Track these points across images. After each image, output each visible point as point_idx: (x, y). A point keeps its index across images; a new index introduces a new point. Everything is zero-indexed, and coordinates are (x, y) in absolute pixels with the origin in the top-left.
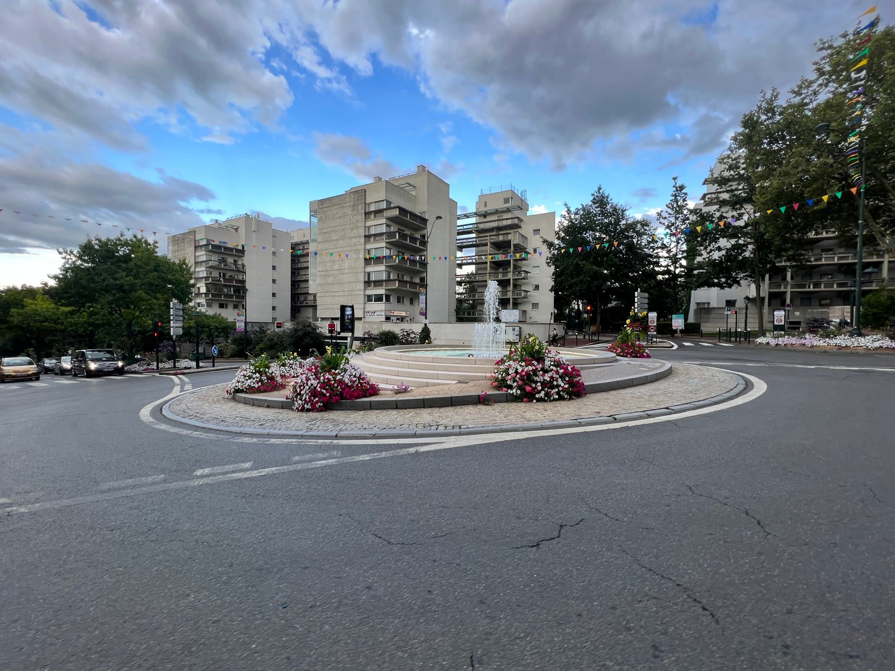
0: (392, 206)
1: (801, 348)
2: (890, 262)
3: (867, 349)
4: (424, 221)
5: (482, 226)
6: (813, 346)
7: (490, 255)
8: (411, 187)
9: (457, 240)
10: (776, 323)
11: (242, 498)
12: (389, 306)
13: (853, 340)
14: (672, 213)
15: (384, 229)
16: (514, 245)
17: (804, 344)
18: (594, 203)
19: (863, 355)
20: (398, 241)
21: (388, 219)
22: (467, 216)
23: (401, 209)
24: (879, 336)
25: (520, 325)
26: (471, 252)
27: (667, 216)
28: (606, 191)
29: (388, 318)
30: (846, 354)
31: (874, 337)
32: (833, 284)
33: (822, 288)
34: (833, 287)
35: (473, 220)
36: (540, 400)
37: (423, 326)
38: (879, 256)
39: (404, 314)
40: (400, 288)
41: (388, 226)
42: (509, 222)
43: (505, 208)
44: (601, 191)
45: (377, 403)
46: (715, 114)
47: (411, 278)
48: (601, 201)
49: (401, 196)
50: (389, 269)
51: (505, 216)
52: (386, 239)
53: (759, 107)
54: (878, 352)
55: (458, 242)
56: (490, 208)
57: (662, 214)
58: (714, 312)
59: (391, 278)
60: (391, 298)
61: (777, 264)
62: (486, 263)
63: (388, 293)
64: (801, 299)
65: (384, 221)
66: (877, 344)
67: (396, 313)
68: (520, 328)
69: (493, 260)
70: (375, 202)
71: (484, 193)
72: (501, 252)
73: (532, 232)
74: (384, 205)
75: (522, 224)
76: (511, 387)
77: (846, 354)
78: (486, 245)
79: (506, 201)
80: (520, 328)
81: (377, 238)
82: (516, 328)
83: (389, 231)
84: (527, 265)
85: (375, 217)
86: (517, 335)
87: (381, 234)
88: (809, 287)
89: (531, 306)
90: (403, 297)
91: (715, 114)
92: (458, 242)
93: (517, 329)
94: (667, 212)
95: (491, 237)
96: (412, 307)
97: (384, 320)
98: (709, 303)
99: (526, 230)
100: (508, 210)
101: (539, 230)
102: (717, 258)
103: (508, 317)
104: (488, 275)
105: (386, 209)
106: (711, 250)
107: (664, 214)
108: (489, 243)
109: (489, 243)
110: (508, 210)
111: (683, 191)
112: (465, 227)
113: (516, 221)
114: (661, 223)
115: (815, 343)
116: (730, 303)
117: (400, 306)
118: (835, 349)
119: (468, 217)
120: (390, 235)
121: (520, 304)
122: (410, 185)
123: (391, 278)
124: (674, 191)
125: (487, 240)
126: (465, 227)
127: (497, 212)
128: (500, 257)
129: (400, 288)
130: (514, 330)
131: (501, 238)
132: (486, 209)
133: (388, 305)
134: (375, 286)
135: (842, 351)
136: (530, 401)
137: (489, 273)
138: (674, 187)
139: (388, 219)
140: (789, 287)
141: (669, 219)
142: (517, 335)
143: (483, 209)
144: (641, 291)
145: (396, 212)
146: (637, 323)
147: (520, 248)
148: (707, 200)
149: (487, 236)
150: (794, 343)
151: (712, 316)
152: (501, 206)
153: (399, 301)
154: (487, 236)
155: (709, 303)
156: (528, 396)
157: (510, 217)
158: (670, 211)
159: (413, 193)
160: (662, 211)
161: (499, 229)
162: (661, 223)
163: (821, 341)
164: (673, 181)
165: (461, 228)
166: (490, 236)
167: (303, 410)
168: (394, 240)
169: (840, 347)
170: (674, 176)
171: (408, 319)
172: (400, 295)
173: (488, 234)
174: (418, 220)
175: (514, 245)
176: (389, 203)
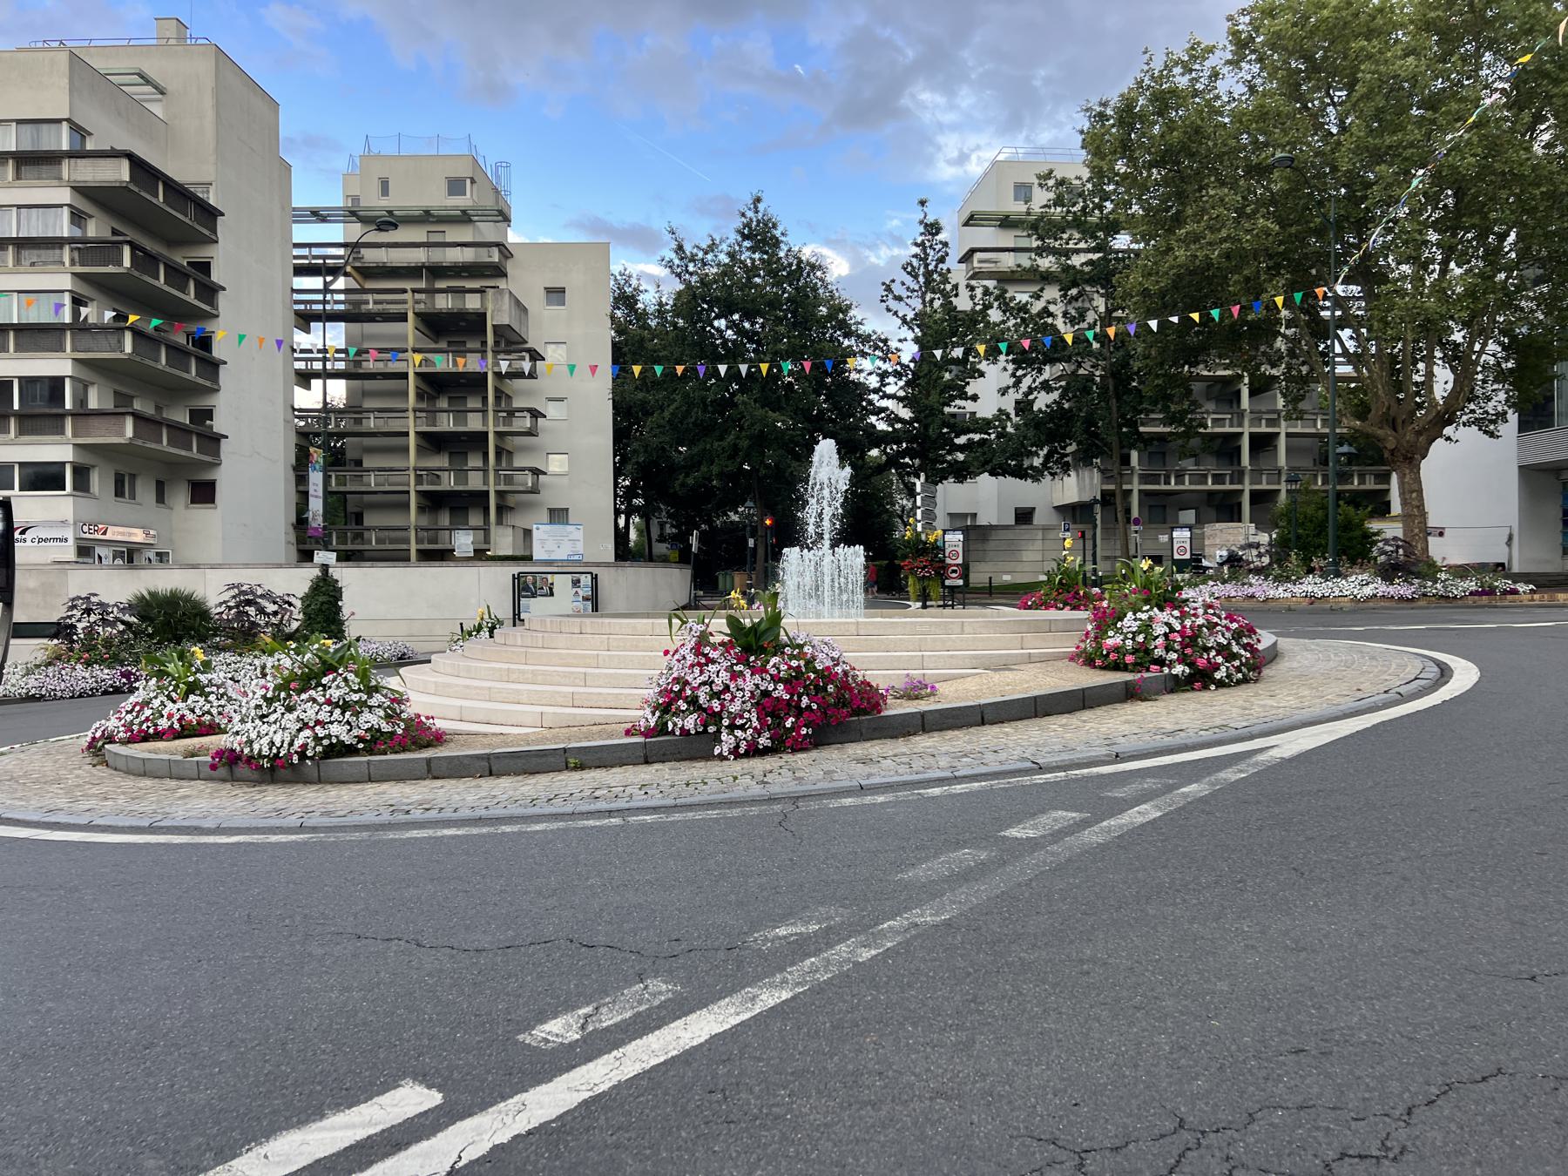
0: (90, 146)
1: (1246, 604)
2: (1288, 435)
3: (1355, 600)
4: (210, 214)
5: (371, 256)
6: (1267, 600)
7: (415, 351)
8: (149, 89)
9: (294, 291)
10: (1176, 556)
11: (193, 1121)
12: (89, 508)
13: (1330, 584)
14: (917, 288)
15: (63, 227)
16: (494, 326)
17: (1253, 596)
18: (745, 237)
19: (1353, 611)
20: (127, 275)
21: (81, 190)
22: (319, 216)
23: (137, 163)
24: (1365, 576)
25: (595, 570)
26: (336, 335)
27: (904, 294)
28: (772, 207)
29: (85, 551)
30: (1324, 611)
31: (1360, 577)
32: (1205, 476)
33: (1187, 486)
34: (1206, 483)
35: (335, 232)
36: (1221, 684)
37: (317, 572)
38: (1271, 422)
39: (138, 536)
40: (139, 442)
41: (78, 217)
42: (467, 256)
43: (455, 208)
44: (761, 206)
45: (937, 715)
46: (887, 33)
47: (158, 408)
48: (761, 235)
49: (119, 114)
50: (85, 374)
51: (454, 234)
52: (73, 263)
53: (1137, 83)
54: (1371, 604)
55: (296, 297)
56: (403, 199)
57: (893, 286)
58: (994, 535)
59: (93, 404)
60: (95, 479)
61: (1142, 429)
62: (404, 376)
63: (85, 460)
64: (1150, 506)
65: (64, 196)
66: (1368, 591)
67: (114, 533)
68: (595, 578)
69: (424, 369)
70: (19, 122)
71: (375, 151)
72: (443, 345)
73: (542, 293)
74: (63, 140)
75: (510, 267)
76: (1161, 662)
77: (1324, 611)
78: (402, 318)
79: (455, 186)
80: (595, 578)
81: (29, 255)
82: (583, 577)
83: (78, 233)
84: (528, 393)
85: (18, 177)
86: (585, 599)
87: (56, 243)
88: (1168, 483)
89: (545, 516)
90: (133, 477)
91: (887, 33)
92: (296, 297)
93: (586, 580)
94: (903, 284)
95: (417, 296)
96: (163, 511)
97: (70, 554)
98: (974, 515)
99: (525, 282)
100: (464, 218)
101: (562, 291)
102: (1044, 409)
103: (551, 545)
104: (411, 415)
105: (72, 155)
106: (1030, 387)
107: (898, 289)
108: (410, 316)
109: (410, 316)
110: (464, 218)
111: (939, 237)
112: (315, 251)
113: (495, 256)
114: (889, 310)
115: (1271, 593)
116: (1024, 516)
117: (123, 507)
118: (1305, 603)
119: (324, 220)
120: (86, 249)
121: (512, 509)
122: (147, 81)
123: (93, 404)
124: (922, 234)
125: (404, 302)
126: (315, 251)
127: (426, 217)
128: (442, 363)
129: (139, 442)
130: (576, 583)
131: (444, 303)
132: (385, 203)
133: (84, 502)
134: (22, 432)
135: (1316, 605)
136: (1205, 687)
137: (415, 411)
138: (921, 222)
139: (81, 190)
140: (1136, 479)
141: (909, 301)
142: (585, 599)
143: (374, 201)
144: (926, 480)
145: (121, 172)
146: (921, 558)
147: (510, 340)
148: (976, 264)
149: (404, 291)
150: (1233, 594)
151: (991, 545)
152: (438, 199)
153: (119, 493)
154: (404, 291)
155: (974, 515)
156: (1201, 678)
157: (469, 239)
158: (909, 280)
159: (157, 109)
160: (893, 281)
161: (437, 271)
162: (889, 310)
163: (1281, 589)
164: (920, 208)
165: (305, 252)
166: (414, 291)
167: (754, 751)
168: (110, 269)
169: (1312, 599)
170: (923, 197)
171: (151, 554)
172: (123, 470)
173: (408, 285)
174: (191, 208)
175: (494, 326)
176: (79, 131)
